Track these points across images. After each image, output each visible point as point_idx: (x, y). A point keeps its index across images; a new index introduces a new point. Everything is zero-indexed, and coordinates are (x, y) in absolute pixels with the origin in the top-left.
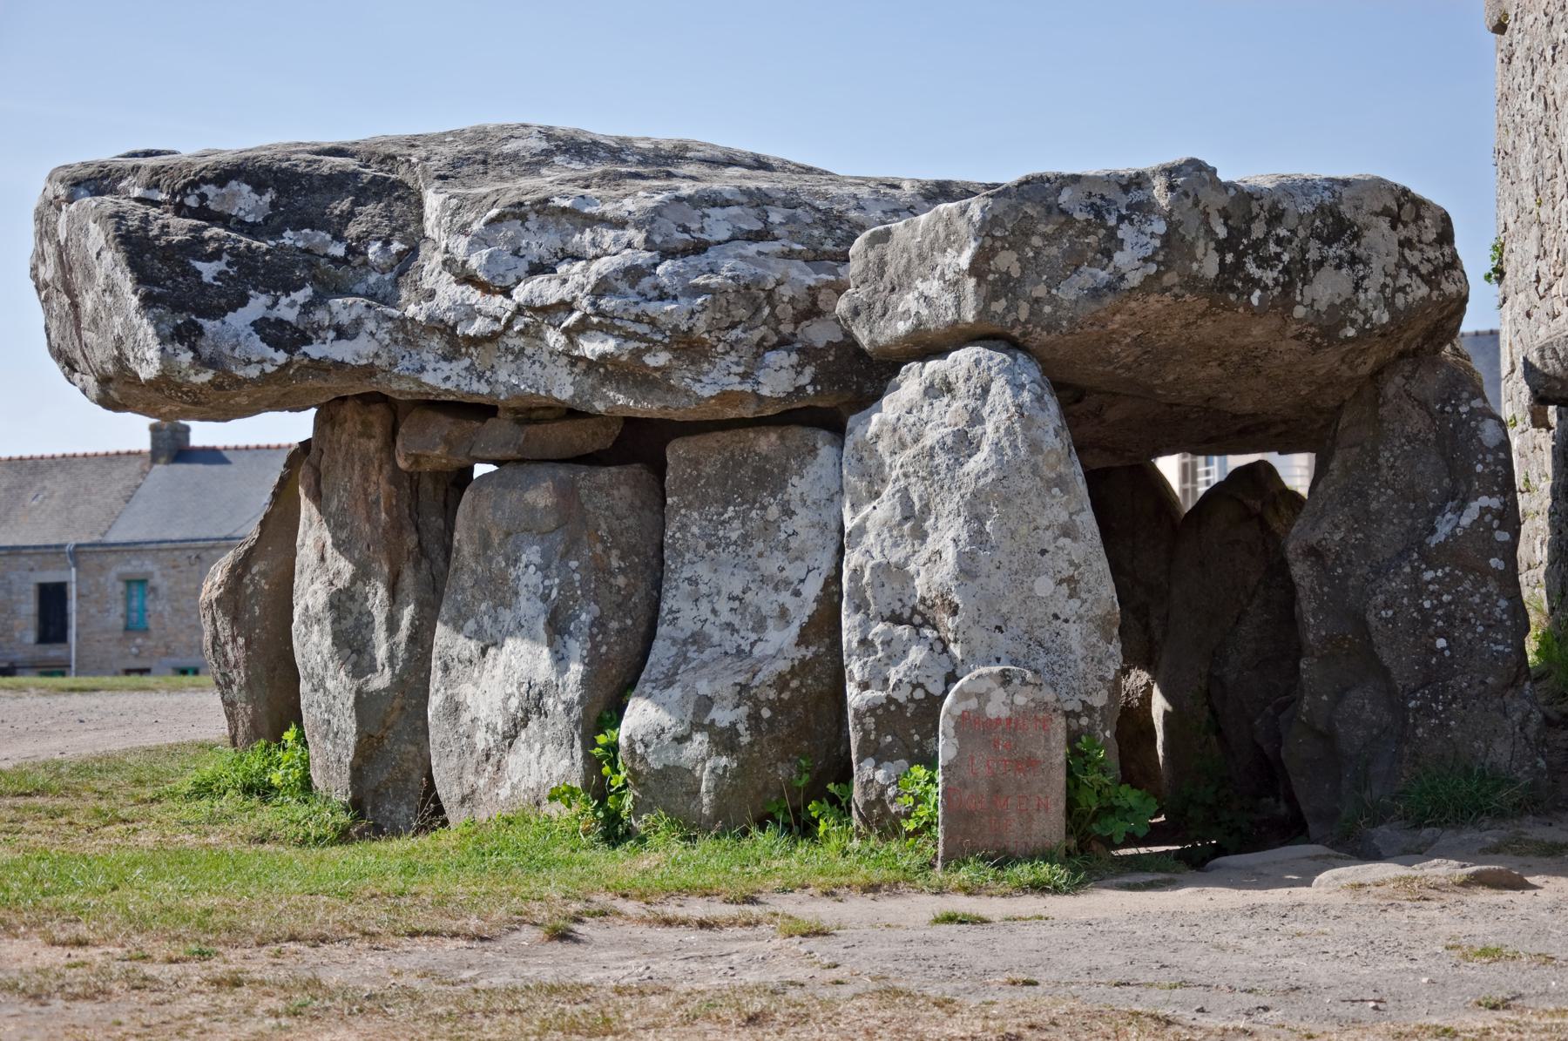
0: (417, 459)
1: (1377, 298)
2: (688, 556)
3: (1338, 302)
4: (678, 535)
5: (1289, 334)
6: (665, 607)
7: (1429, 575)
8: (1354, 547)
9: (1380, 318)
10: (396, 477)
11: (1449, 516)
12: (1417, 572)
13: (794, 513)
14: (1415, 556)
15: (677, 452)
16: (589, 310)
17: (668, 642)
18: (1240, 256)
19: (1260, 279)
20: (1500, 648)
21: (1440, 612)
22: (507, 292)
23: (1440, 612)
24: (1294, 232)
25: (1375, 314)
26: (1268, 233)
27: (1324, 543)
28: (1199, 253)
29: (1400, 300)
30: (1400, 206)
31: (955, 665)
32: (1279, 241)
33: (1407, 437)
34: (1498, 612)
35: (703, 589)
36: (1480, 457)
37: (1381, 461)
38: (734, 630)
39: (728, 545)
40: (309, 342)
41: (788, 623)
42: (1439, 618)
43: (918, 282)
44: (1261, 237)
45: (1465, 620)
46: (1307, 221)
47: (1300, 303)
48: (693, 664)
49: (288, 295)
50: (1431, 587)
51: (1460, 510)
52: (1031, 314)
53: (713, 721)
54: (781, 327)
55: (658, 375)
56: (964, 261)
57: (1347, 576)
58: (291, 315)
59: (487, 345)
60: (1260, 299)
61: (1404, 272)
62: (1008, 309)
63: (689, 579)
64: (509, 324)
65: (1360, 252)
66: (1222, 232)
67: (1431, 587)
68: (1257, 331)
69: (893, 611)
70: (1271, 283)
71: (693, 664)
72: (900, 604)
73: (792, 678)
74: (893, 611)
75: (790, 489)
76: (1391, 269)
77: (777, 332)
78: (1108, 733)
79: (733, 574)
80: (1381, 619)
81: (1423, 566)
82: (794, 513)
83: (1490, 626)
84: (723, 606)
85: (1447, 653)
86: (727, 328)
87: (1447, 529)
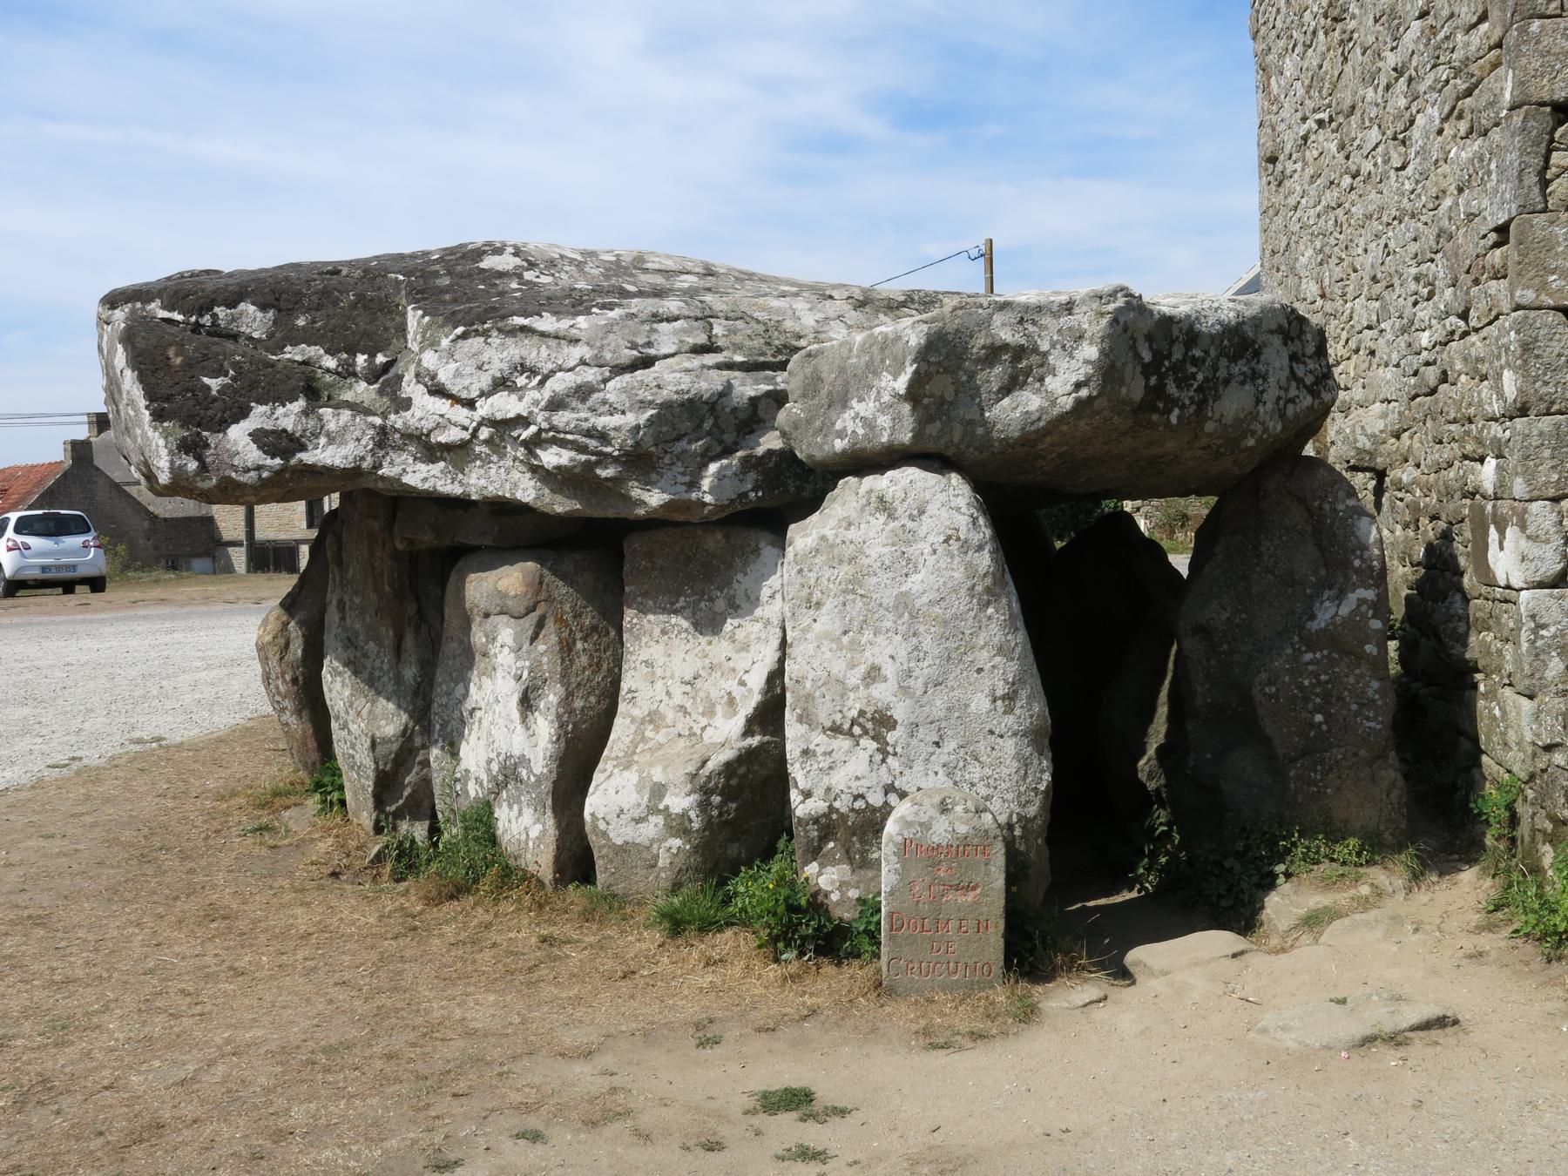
0: (411, 542)
2: (644, 640)
3: (1242, 416)
4: (635, 621)
5: (1197, 445)
6: (624, 686)
7: (1308, 657)
9: (1275, 427)
10: (396, 556)
11: (1327, 604)
12: (1298, 653)
13: (739, 607)
14: (1296, 639)
15: (634, 546)
16: (545, 425)
17: (628, 721)
18: (1161, 378)
19: (1178, 399)
20: (1373, 724)
21: (1318, 690)
22: (470, 404)
23: (1318, 690)
24: (1206, 352)
25: (1271, 424)
28: (1128, 375)
29: (1290, 410)
30: (1290, 323)
31: (895, 777)
32: (1195, 362)
34: (1370, 693)
35: (659, 672)
36: (1358, 553)
37: (1263, 549)
38: (686, 713)
39: (680, 633)
40: (303, 448)
41: (735, 713)
42: (1317, 695)
43: (854, 403)
44: (1181, 358)
45: (1340, 698)
46: (1217, 342)
47: (1210, 419)
48: (650, 744)
49: (284, 406)
50: (1310, 668)
51: (1340, 597)
52: (964, 435)
53: (667, 808)
54: (725, 437)
55: (609, 484)
56: (901, 384)
58: (288, 424)
59: (459, 451)
60: (1179, 417)
61: (1294, 384)
63: (646, 662)
64: (475, 434)
65: (1261, 368)
66: (1147, 356)
67: (1310, 668)
68: (1170, 445)
69: (834, 722)
70: (1187, 402)
71: (650, 744)
72: (840, 715)
73: (740, 766)
74: (834, 722)
75: (735, 585)
76: (1283, 383)
77: (721, 442)
78: (1040, 841)
79: (684, 660)
81: (1304, 649)
82: (739, 607)
84: (678, 690)
85: (1324, 727)
87: (1328, 616)
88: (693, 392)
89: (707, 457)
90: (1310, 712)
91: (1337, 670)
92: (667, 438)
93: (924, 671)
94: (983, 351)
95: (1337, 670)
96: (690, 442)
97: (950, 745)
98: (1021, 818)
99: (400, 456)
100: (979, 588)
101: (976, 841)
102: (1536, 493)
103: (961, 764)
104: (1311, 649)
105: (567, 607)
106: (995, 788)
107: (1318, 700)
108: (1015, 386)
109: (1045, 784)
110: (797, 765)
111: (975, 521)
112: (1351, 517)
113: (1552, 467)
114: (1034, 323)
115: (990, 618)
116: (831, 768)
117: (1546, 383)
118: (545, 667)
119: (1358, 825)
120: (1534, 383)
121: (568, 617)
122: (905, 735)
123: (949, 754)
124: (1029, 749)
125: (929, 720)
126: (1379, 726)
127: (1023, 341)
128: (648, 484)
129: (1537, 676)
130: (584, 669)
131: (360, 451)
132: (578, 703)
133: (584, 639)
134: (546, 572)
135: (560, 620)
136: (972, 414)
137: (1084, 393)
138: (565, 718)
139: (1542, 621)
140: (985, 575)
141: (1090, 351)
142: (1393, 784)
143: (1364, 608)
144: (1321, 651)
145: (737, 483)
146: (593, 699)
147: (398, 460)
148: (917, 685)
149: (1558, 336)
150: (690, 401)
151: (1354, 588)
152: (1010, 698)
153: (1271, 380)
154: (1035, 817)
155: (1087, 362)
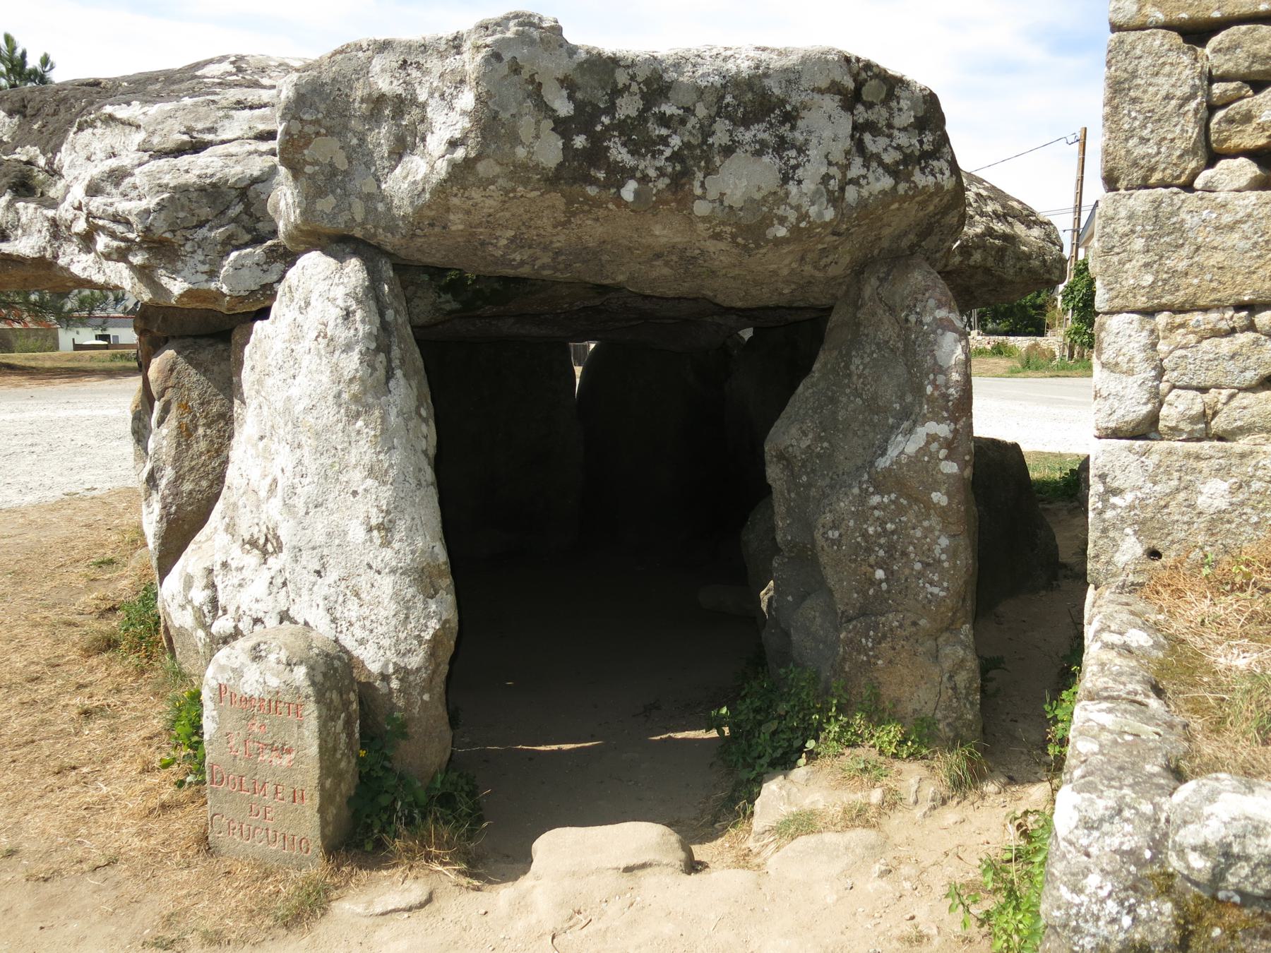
1: (817, 192)
7: (876, 499)
8: (819, 456)
9: (820, 214)
12: (865, 495)
14: (866, 477)
20: (936, 590)
21: (882, 541)
23: (882, 541)
25: (813, 211)
26: (647, 108)
27: (790, 449)
32: (664, 120)
33: (878, 344)
34: (937, 551)
36: (931, 376)
37: (853, 368)
42: (881, 546)
44: (634, 114)
45: (904, 554)
50: (877, 513)
57: (809, 486)
60: (637, 193)
62: (338, 209)
66: (564, 108)
70: (652, 173)
76: (838, 156)
80: (827, 539)
81: (871, 489)
83: (928, 565)
85: (884, 586)
86: (195, 227)
88: (219, 175)
89: (229, 244)
90: (871, 566)
91: (904, 519)
92: (186, 225)
93: (307, 489)
94: (364, 106)
95: (904, 519)
96: (211, 230)
97: (332, 575)
98: (398, 669)
99: (70, 247)
100: (345, 396)
101: (287, 698)
102: (1118, 303)
103: (341, 599)
104: (879, 490)
105: (195, 394)
106: (371, 631)
107: (881, 553)
108: (405, 149)
109: (431, 632)
110: (220, 577)
111: (348, 315)
112: (934, 332)
113: (1146, 265)
114: (419, 66)
115: (359, 432)
116: (240, 585)
117: (1144, 141)
118: (164, 450)
119: (910, 709)
120: (1127, 140)
121: (195, 404)
122: (289, 560)
123: (329, 586)
124: (411, 590)
125: (311, 545)
126: (942, 594)
127: (400, 91)
128: (174, 272)
129: (1103, 558)
130: (201, 454)
131: (42, 243)
132: (187, 487)
133: (208, 426)
134: (180, 359)
135: (185, 407)
136: (370, 187)
137: (460, 153)
138: (169, 500)
139: (1115, 485)
140: (351, 381)
141: (467, 100)
142: (961, 664)
143: (934, 446)
144: (889, 494)
145: (259, 273)
146: (204, 483)
147: (68, 251)
148: (299, 503)
149: (1167, 69)
150: (213, 185)
151: (925, 420)
152: (386, 528)
153: (812, 153)
154: (418, 670)
155: (464, 113)
